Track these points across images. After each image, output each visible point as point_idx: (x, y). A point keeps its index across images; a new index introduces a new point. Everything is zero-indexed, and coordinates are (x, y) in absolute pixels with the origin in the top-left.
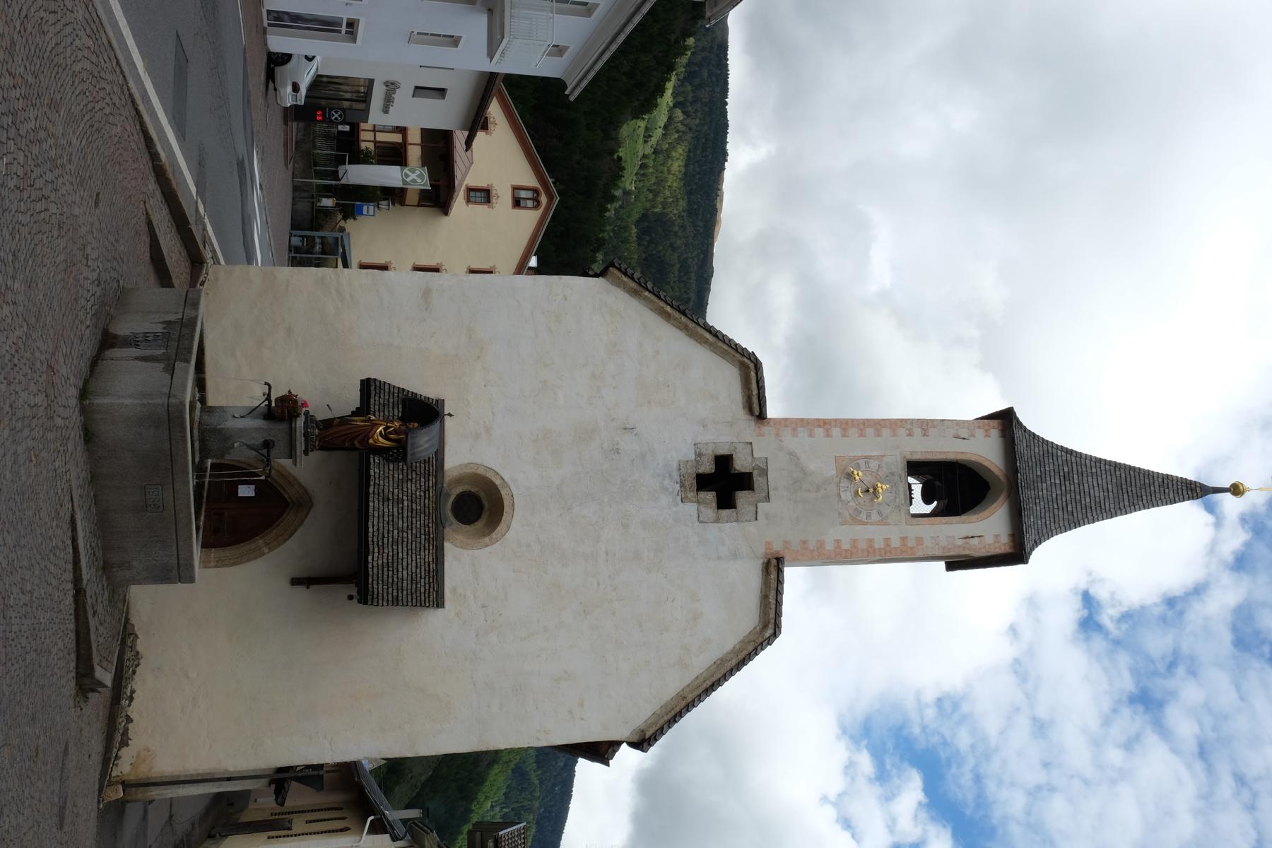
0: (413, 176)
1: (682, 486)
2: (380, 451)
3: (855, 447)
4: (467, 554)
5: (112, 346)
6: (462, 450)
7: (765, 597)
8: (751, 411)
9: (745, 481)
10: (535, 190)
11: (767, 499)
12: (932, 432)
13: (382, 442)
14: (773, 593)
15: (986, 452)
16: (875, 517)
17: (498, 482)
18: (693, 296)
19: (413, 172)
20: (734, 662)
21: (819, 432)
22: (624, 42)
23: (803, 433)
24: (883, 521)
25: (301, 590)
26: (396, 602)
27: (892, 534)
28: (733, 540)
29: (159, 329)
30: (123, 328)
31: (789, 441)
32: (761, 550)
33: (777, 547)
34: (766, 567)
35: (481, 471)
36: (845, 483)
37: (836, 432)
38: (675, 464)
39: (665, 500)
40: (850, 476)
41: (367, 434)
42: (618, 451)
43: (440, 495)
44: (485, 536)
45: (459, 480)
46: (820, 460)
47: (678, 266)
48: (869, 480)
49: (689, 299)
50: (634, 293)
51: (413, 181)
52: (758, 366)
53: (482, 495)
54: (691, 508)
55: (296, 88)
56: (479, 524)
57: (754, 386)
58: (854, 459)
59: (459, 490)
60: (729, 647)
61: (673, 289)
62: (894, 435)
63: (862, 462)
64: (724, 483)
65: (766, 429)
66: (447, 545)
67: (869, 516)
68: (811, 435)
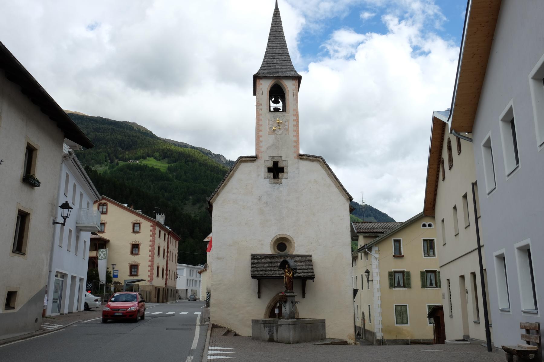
0: (102, 255)
1: (277, 183)
2: (293, 274)
3: (265, 128)
4: (296, 248)
5: (273, 339)
6: (267, 249)
7: (310, 160)
8: (255, 160)
9: (276, 163)
10: (99, 205)
11: (281, 157)
12: (260, 102)
14: (309, 158)
15: (266, 86)
16: (287, 123)
18: (111, 127)
19: (100, 255)
20: (329, 171)
21: (261, 139)
22: (93, 182)
23: (261, 144)
24: (288, 121)
25: (306, 295)
26: (312, 269)
27: (292, 118)
28: (295, 170)
29: (267, 329)
30: (267, 337)
31: (264, 149)
32: (296, 160)
33: (296, 155)
34: (301, 159)
35: (272, 243)
36: (276, 132)
37: (261, 133)
38: (271, 185)
39: (281, 189)
40: (274, 130)
41: (289, 278)
42: (267, 202)
43: (279, 255)
46: (269, 139)
47: (96, 133)
48: (276, 125)
49: (112, 128)
50: (218, 195)
51: (104, 255)
52: (241, 158)
54: (284, 181)
55: (96, 300)
56: (287, 244)
57: (247, 159)
58: (269, 128)
59: (276, 250)
60: (324, 172)
61: (107, 136)
62: (262, 115)
63: (270, 126)
64: (276, 170)
65: (260, 156)
67: (286, 125)
68: (262, 142)
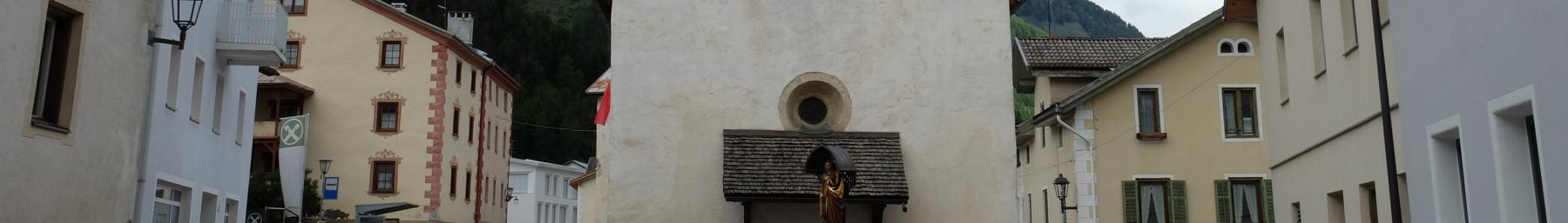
0: (292, 133)
2: (846, 190)
4: (856, 113)
13: (841, 188)
17: (795, 85)
19: (286, 133)
26: (901, 173)
35: (786, 99)
43: (804, 134)
44: (840, 97)
45: (791, 118)
51: (298, 133)
53: (802, 98)
56: (827, 101)
59: (797, 117)
66: (847, 130)
